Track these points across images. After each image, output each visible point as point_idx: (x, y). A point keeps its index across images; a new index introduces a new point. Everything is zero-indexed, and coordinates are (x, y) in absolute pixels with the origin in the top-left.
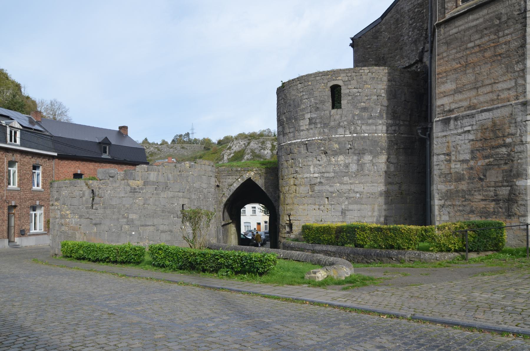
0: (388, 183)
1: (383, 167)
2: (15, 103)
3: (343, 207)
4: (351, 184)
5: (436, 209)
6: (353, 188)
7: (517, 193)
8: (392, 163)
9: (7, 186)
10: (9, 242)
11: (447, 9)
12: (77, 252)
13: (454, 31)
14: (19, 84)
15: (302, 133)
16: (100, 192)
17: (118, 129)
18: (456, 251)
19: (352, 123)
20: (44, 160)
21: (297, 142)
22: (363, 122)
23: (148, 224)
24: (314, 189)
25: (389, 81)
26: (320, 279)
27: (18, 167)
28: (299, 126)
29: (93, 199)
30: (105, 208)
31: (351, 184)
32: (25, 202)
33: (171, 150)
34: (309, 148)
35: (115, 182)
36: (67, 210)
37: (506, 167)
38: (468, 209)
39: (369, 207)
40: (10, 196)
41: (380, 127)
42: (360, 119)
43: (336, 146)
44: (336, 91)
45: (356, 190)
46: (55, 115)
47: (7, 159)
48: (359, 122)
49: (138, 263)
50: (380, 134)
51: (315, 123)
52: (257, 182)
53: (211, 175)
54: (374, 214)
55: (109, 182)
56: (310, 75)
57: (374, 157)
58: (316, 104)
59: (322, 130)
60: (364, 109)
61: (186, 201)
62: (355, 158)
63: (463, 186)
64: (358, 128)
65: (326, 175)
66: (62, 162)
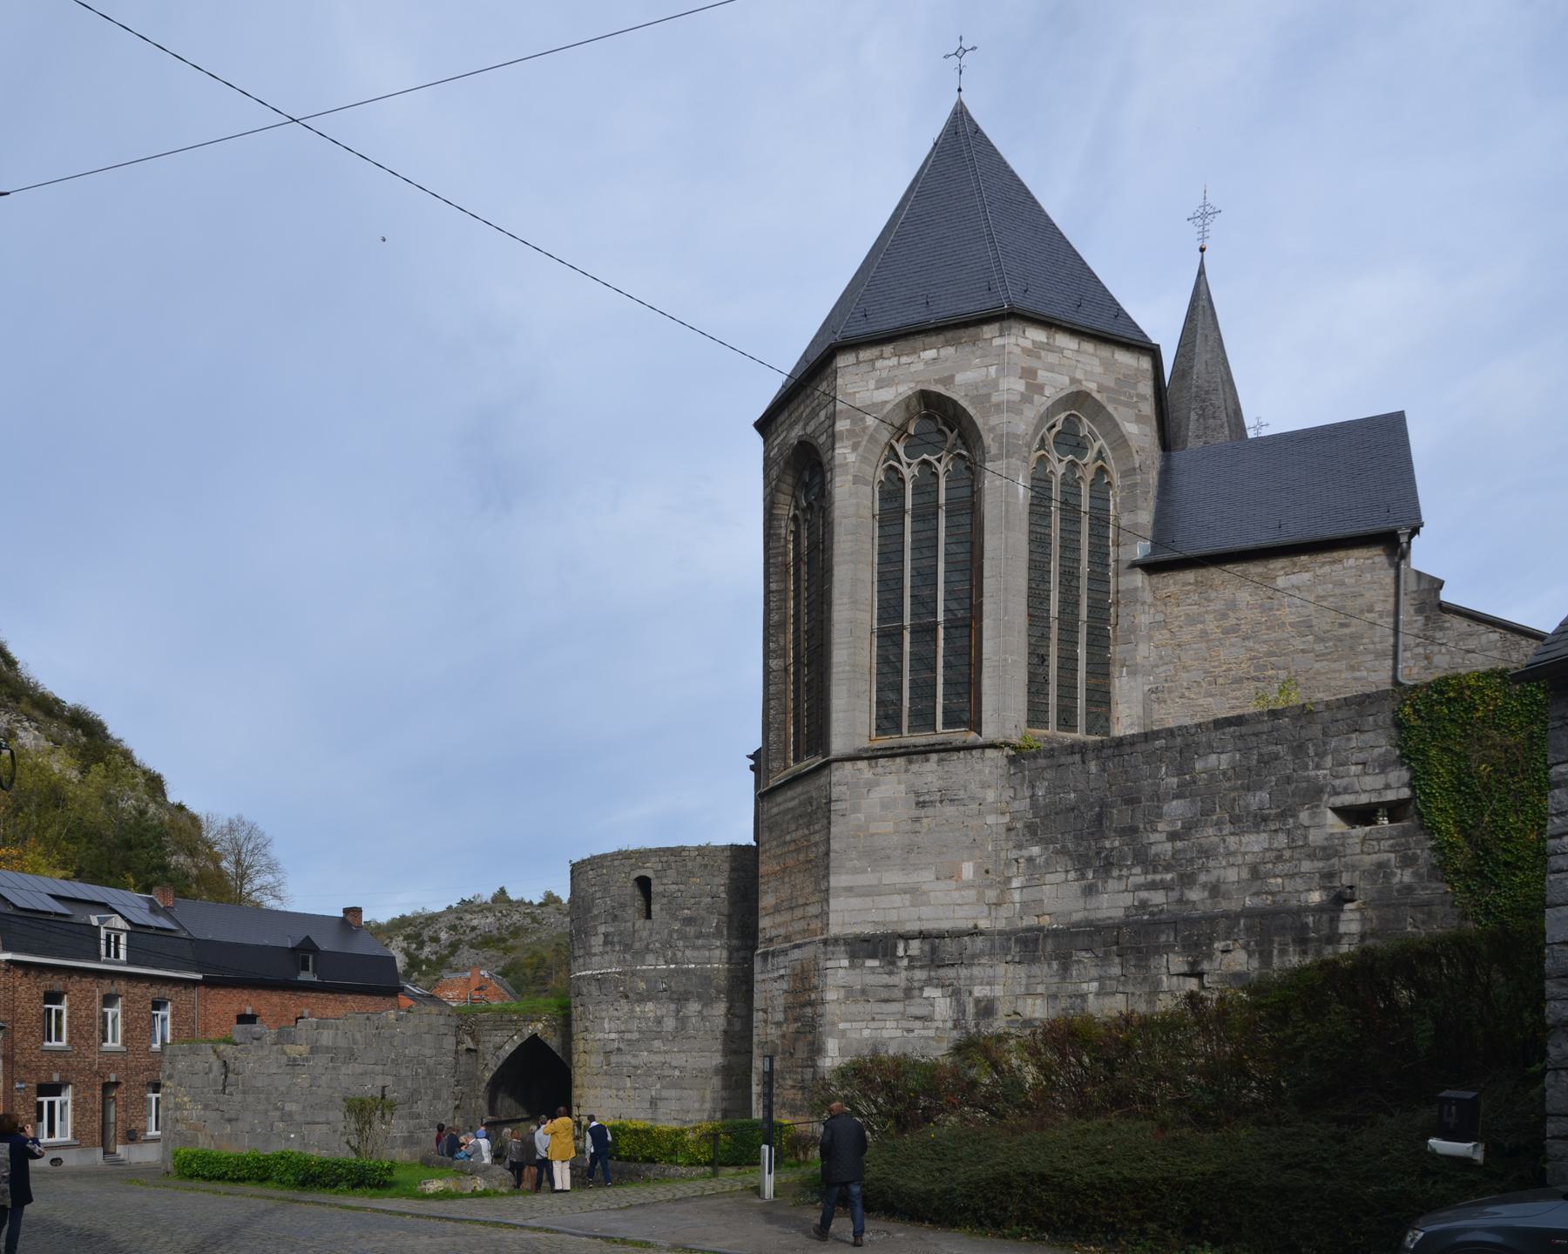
1: (720, 1023)
2: (146, 830)
3: (653, 1093)
4: (666, 1052)
8: (736, 1016)
9: (100, 1045)
10: (104, 1153)
11: (771, 771)
13: (775, 810)
17: (341, 915)
18: (707, 1164)
20: (177, 989)
21: (586, 975)
22: (687, 944)
23: (317, 1120)
25: (733, 870)
27: (123, 1006)
28: (590, 946)
29: (226, 1077)
30: (244, 1092)
31: (666, 1052)
32: (137, 1075)
37: (810, 1037)
40: (106, 1064)
41: (717, 952)
42: (681, 939)
43: (642, 985)
44: (644, 884)
45: (674, 1063)
47: (100, 992)
48: (680, 943)
50: (716, 965)
51: (612, 943)
52: (548, 1042)
53: (446, 1031)
54: (704, 1107)
56: (604, 856)
57: (703, 1006)
58: (613, 908)
60: (689, 921)
61: (389, 1081)
62: (673, 1007)
64: (679, 954)
65: (627, 1036)
66: (213, 992)
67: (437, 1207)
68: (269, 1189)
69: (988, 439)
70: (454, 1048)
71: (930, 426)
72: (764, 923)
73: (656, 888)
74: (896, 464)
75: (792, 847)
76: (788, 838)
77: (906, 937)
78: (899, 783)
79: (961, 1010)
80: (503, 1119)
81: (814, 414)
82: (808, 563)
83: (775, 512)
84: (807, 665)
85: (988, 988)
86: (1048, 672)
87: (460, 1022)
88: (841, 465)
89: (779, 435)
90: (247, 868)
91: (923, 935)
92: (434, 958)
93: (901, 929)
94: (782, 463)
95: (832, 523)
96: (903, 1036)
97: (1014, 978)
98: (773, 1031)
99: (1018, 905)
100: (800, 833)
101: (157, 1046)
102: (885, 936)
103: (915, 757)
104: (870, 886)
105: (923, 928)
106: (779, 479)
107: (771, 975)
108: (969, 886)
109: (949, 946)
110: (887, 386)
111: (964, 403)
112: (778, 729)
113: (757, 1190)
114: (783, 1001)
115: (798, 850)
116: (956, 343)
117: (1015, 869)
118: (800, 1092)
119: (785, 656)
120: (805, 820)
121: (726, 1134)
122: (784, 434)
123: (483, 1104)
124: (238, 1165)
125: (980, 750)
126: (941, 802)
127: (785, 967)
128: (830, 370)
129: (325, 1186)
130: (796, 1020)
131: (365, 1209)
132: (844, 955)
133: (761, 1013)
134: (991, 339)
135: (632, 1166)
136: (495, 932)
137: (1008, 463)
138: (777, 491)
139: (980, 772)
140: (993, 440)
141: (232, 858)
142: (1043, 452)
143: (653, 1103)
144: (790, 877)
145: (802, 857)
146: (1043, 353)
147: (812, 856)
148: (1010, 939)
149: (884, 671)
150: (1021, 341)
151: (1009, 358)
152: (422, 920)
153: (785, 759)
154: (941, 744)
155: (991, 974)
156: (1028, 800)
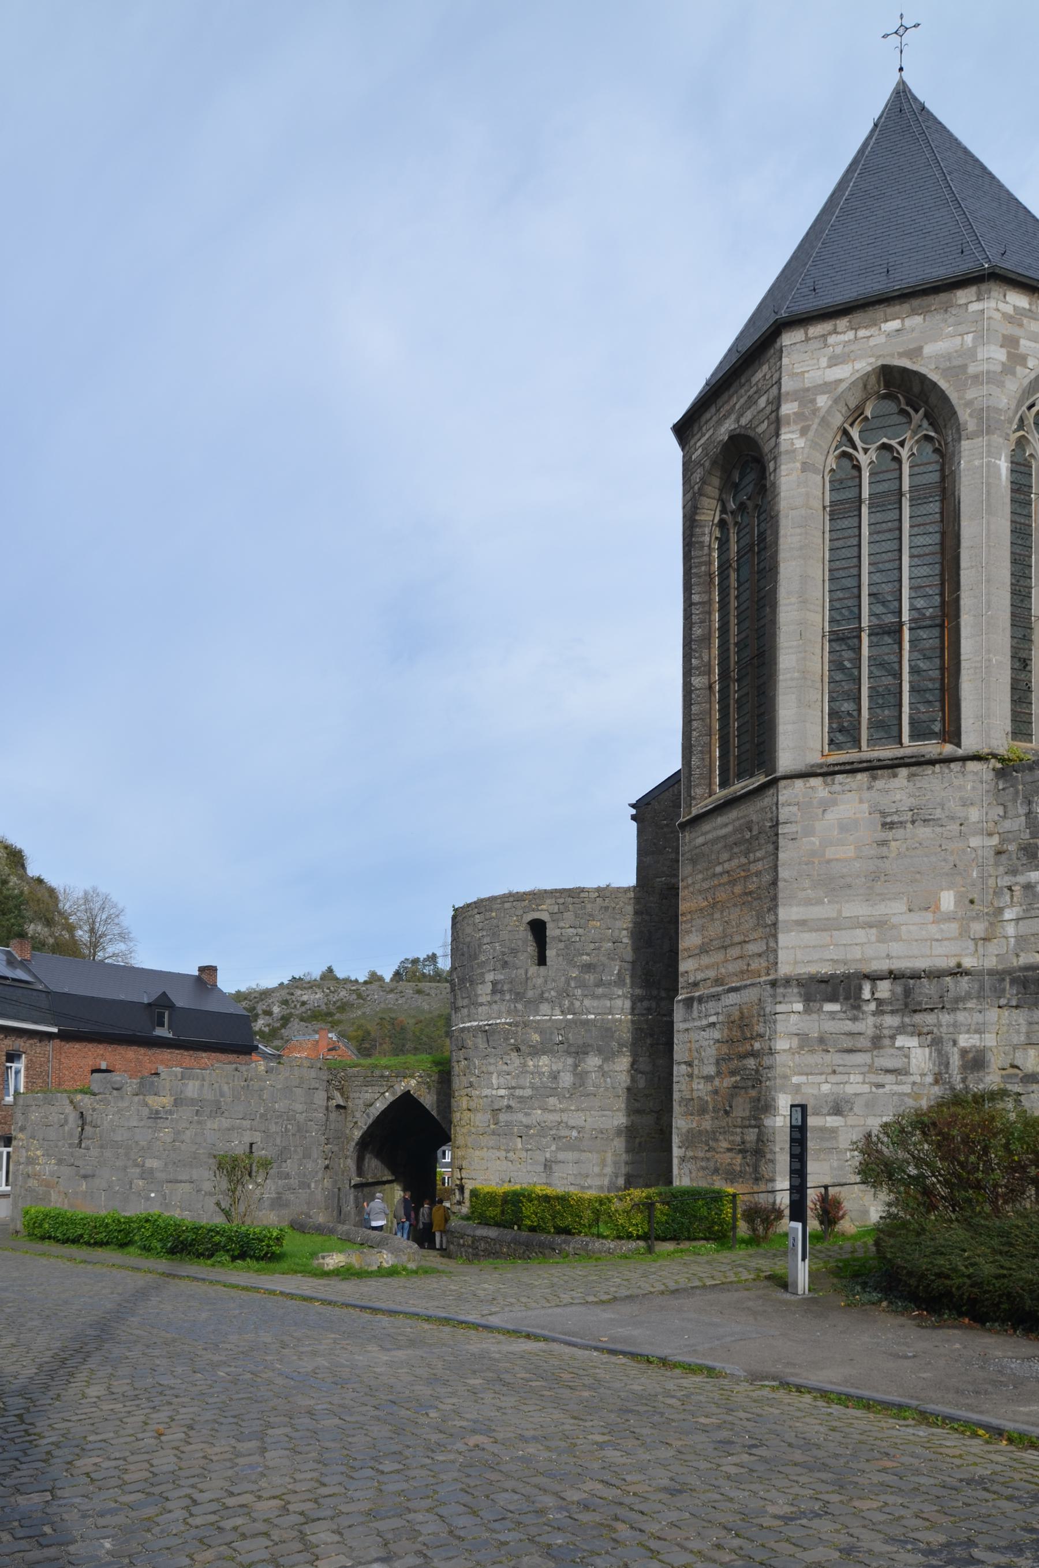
0: (632, 1111)
2: (7, 898)
3: (548, 1155)
4: (562, 1111)
5: (675, 1162)
6: (565, 1119)
7: (765, 1139)
11: (695, 799)
12: (41, 1226)
13: (700, 840)
14: (20, 852)
15: (480, 1009)
16: (95, 1116)
17: (197, 973)
18: (639, 1238)
19: (565, 993)
20: (31, 1041)
21: (471, 1027)
22: (586, 992)
23: (180, 1178)
24: (498, 1119)
25: (637, 913)
26: (331, 1268)
28: (477, 996)
30: (102, 1147)
31: (562, 1111)
33: (391, 996)
34: (490, 1038)
35: (122, 1098)
36: (37, 1149)
37: (753, 1093)
38: (711, 1164)
39: (594, 1157)
41: (619, 1003)
43: (536, 1037)
44: (538, 928)
45: (571, 1123)
46: (94, 922)
49: (123, 1245)
51: (502, 992)
52: (421, 1100)
53: (317, 1086)
54: (605, 1171)
55: (110, 1098)
56: (492, 899)
59: (512, 1006)
60: (588, 967)
61: (257, 1137)
62: (570, 1061)
63: (707, 1124)
64: (577, 1004)
65: (519, 1092)
67: (348, 1290)
68: (132, 1256)
69: (964, 415)
70: (325, 1104)
71: (890, 406)
72: (683, 967)
73: (551, 932)
74: (851, 450)
75: (725, 879)
76: (719, 869)
77: (874, 978)
78: (861, 801)
79: (944, 1063)
80: (370, 1180)
81: (751, 402)
82: (738, 570)
83: (697, 518)
84: (738, 680)
85: (977, 1036)
86: (1030, 677)
87: (331, 1077)
88: (787, 452)
89: (703, 435)
90: (100, 937)
91: (893, 976)
92: (267, 1029)
93: (867, 969)
94: (707, 464)
95: (777, 515)
96: (871, 1092)
97: (1009, 1025)
98: (701, 1087)
99: (1012, 940)
100: (735, 862)
101: (9, 1099)
102: (847, 977)
103: (879, 772)
104: (827, 919)
105: (893, 967)
106: (704, 481)
107: (698, 1024)
108: (950, 918)
109: (927, 989)
110: (841, 363)
111: (934, 377)
112: (701, 752)
113: (783, 1283)
114: (714, 1052)
115: (733, 882)
116: (925, 312)
117: (1008, 898)
118: (740, 1156)
119: (709, 673)
120: (743, 848)
121: (663, 1203)
122: (711, 432)
123: (351, 1164)
124: (95, 1227)
125: (960, 763)
126: (913, 822)
127: (717, 1014)
128: (772, 351)
129: (199, 1255)
130: (733, 1073)
131: (256, 1289)
132: (799, 999)
133: (684, 1067)
134: (967, 304)
135: (543, 1237)
136: (324, 1007)
137: (989, 440)
138: (701, 495)
139: (961, 788)
140: (971, 415)
141: (86, 928)
142: (1022, 433)
143: (548, 1166)
144: (722, 912)
145: (738, 889)
146: (1025, 321)
147: (752, 887)
148: (1003, 980)
149: (838, 679)
150: (1002, 306)
151: (989, 324)
152: (257, 995)
153: (710, 785)
154: (912, 757)
155: (981, 1021)
156: (1023, 818)
